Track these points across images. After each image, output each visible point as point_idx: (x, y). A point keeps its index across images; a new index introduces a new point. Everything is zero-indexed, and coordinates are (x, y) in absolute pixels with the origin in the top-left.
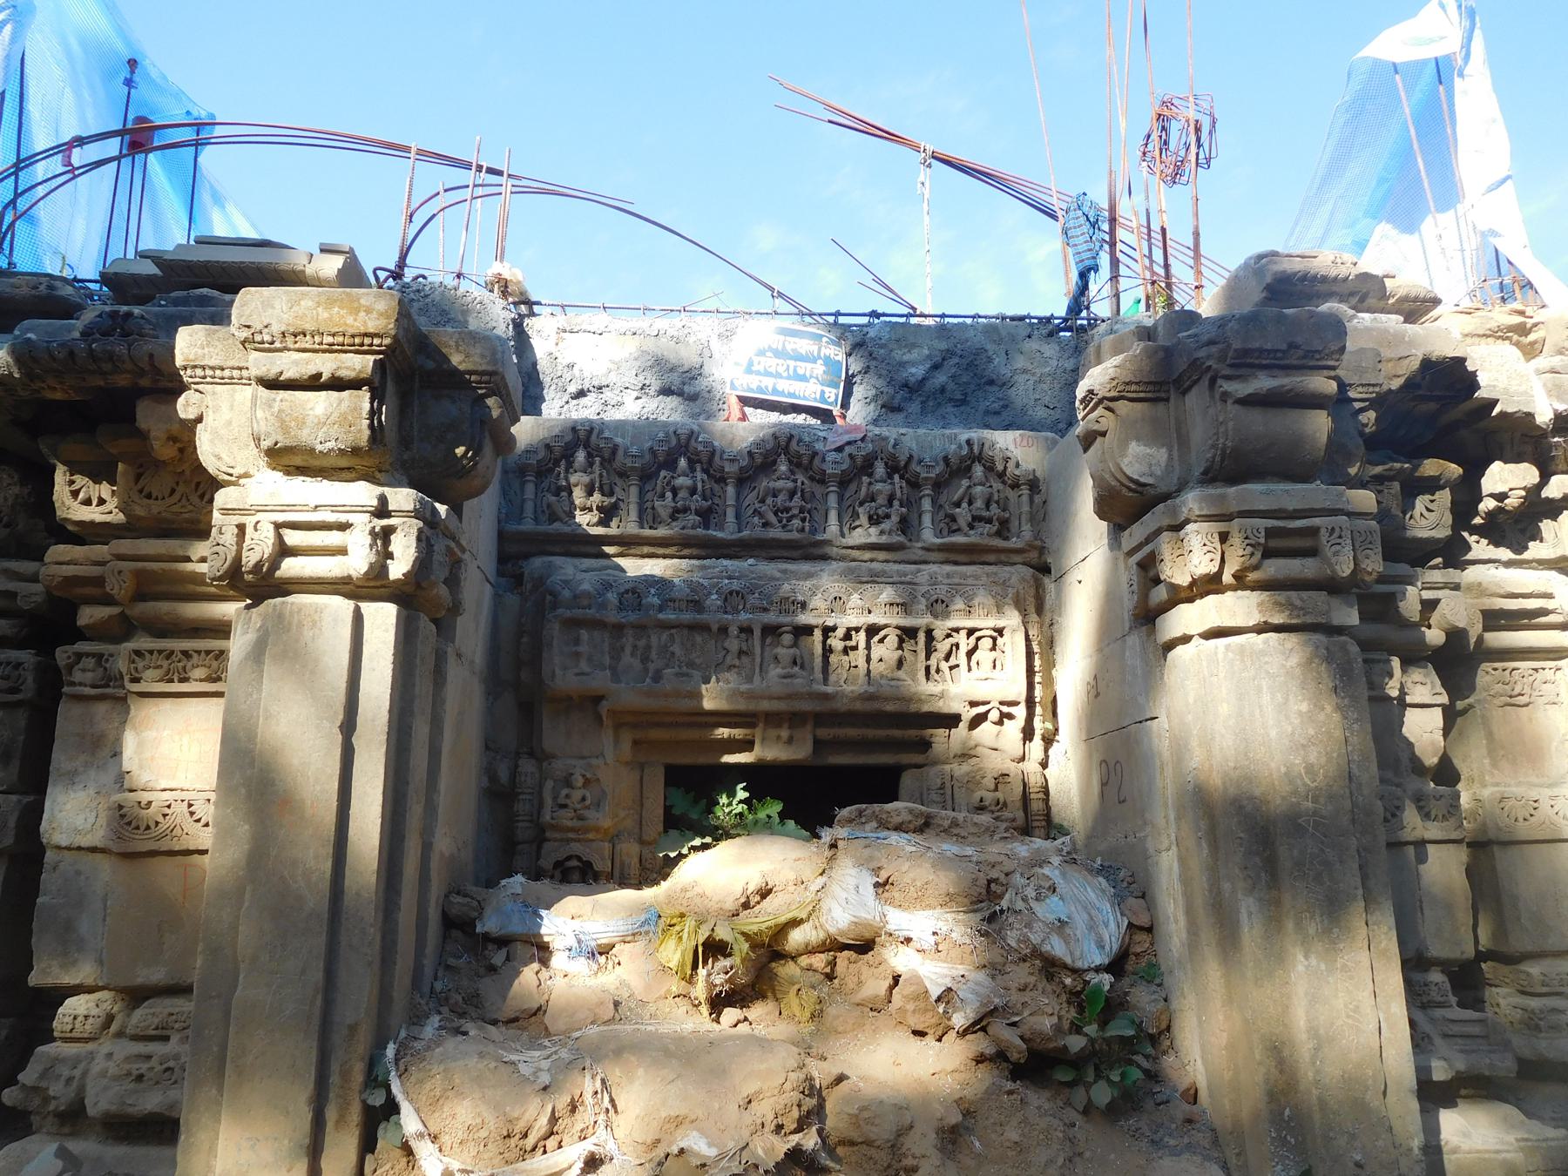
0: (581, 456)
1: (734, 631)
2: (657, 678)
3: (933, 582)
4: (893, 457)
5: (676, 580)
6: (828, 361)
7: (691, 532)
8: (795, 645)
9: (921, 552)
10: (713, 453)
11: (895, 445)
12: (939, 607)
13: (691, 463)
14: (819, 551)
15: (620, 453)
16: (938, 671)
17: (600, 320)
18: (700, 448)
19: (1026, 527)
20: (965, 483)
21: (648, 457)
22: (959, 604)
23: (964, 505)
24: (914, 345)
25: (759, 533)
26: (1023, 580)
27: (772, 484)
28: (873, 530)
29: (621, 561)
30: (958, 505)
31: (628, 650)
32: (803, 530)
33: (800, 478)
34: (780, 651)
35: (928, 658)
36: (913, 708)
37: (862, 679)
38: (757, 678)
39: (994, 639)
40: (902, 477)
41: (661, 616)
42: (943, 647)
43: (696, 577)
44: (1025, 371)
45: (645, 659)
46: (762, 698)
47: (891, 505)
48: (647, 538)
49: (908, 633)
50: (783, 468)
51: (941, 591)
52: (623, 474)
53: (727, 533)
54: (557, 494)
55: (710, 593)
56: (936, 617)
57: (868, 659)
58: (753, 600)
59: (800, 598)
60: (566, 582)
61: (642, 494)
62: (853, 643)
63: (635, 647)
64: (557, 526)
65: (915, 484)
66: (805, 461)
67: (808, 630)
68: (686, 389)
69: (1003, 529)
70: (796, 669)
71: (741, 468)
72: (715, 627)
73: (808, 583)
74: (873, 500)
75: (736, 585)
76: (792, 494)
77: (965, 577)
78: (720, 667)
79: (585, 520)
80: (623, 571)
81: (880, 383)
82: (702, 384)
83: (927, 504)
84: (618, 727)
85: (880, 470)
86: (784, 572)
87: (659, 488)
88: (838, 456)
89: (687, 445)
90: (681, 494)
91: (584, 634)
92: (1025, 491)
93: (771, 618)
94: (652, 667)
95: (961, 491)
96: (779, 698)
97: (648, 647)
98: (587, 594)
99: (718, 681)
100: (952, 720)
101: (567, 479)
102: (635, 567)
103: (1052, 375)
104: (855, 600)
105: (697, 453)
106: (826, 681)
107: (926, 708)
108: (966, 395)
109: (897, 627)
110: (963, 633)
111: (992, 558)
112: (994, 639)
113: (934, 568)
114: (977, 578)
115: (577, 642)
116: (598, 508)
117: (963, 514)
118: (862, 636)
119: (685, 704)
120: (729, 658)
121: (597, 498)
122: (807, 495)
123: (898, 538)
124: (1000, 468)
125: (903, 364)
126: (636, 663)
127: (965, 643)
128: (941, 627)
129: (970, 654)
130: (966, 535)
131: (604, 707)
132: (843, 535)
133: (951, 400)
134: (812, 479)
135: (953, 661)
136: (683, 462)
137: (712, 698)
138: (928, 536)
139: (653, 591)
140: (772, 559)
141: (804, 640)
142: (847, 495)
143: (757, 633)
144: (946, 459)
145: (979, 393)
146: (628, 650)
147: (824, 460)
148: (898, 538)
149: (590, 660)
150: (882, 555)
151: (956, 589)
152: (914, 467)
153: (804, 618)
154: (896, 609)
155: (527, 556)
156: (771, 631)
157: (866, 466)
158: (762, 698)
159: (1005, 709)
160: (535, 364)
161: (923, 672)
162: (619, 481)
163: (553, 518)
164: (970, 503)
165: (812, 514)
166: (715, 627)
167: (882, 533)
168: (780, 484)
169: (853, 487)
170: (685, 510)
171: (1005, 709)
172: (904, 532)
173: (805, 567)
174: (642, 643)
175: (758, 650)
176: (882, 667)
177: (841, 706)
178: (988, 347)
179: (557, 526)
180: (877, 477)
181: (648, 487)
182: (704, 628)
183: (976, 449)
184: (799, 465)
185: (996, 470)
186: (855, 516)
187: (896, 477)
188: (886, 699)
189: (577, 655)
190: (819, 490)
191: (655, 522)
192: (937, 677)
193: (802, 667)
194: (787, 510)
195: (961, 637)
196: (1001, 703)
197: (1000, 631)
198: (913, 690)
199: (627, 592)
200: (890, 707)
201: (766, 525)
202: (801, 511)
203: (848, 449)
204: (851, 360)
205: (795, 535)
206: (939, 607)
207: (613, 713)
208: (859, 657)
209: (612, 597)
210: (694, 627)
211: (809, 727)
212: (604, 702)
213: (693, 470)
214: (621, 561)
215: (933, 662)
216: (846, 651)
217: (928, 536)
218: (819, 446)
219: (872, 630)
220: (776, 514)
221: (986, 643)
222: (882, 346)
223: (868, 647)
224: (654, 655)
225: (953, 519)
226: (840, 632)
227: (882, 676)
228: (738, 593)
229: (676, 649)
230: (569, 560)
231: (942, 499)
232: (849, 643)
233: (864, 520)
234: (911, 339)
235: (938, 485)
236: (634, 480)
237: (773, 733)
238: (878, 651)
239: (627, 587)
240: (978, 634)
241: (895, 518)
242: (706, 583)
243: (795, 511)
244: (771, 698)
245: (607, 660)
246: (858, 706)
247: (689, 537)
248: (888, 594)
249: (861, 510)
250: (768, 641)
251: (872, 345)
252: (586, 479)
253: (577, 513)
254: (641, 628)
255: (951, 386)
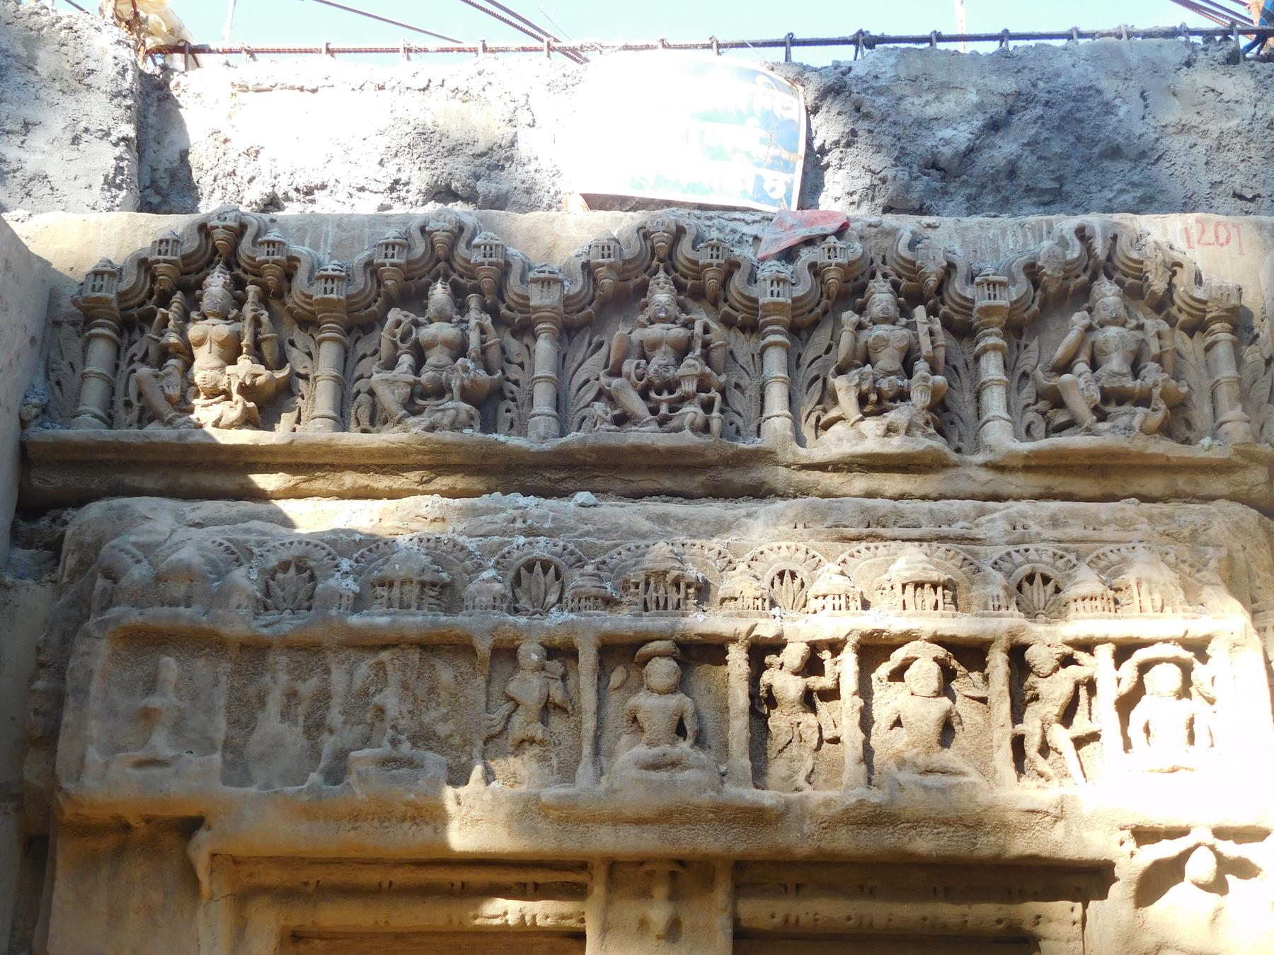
0: (216, 284)
1: (531, 653)
2: (337, 772)
3: (1019, 536)
4: (912, 269)
5: (402, 540)
6: (768, 119)
7: (448, 436)
8: (681, 686)
9: (984, 475)
10: (506, 268)
11: (912, 245)
12: (1036, 588)
13: (459, 294)
14: (740, 478)
15: (302, 274)
16: (1045, 749)
17: (314, 69)
18: (477, 257)
19: (1233, 414)
20: (1079, 319)
21: (361, 280)
22: (1087, 582)
23: (1081, 367)
24: (946, 87)
25: (595, 431)
26: (1238, 528)
27: (638, 335)
28: (872, 426)
29: (289, 507)
30: (1065, 367)
31: (275, 703)
32: (706, 428)
33: (701, 318)
34: (645, 702)
35: (1017, 715)
36: (986, 846)
37: (852, 769)
38: (585, 770)
39: (1186, 669)
40: (932, 312)
41: (355, 620)
42: (1055, 689)
43: (453, 530)
44: (1184, 129)
45: (316, 727)
46: (596, 819)
47: (909, 373)
48: (350, 452)
49: (965, 654)
50: (661, 296)
51: (1041, 557)
52: (308, 323)
53: (536, 435)
54: (160, 364)
55: (480, 568)
56: (1031, 614)
57: (866, 722)
58: (578, 580)
59: (693, 573)
60: (148, 549)
61: (347, 361)
62: (825, 682)
63: (292, 695)
64: (155, 431)
65: (962, 329)
66: (711, 280)
67: (710, 650)
68: (482, 186)
69: (1177, 421)
70: (684, 746)
71: (567, 300)
72: (484, 646)
73: (717, 543)
74: (867, 360)
75: (542, 547)
76: (682, 351)
77: (1097, 524)
78: (494, 742)
79: (217, 421)
80: (287, 523)
81: (880, 162)
82: (514, 177)
83: (992, 368)
84: (244, 897)
85: (881, 296)
86: (663, 519)
87: (385, 350)
88: (786, 271)
89: (449, 260)
90: (434, 357)
91: (170, 666)
92: (1222, 334)
93: (623, 621)
94: (329, 744)
95: (1073, 336)
96: (639, 821)
97: (323, 698)
98: (186, 572)
99: (489, 776)
100: (1090, 879)
101: (182, 333)
102: (315, 515)
103: (1246, 134)
104: (828, 579)
105: (470, 272)
106: (759, 775)
107: (1020, 846)
108: (1060, 179)
109: (938, 640)
110: (1105, 653)
111: (1155, 484)
112: (1186, 669)
113: (1015, 507)
114: (1125, 524)
115: (152, 685)
116: (243, 389)
117: (1080, 388)
118: (849, 658)
119: (405, 839)
120: (518, 720)
121: (244, 367)
122: (717, 355)
123: (924, 443)
124: (1158, 285)
125: (924, 124)
126: (294, 736)
127: (1112, 680)
128: (1044, 642)
129: (1126, 705)
130: (1089, 431)
131: (202, 848)
132: (800, 441)
133: (1029, 190)
134: (728, 322)
135: (1081, 725)
136: (439, 293)
137: (475, 818)
138: (1000, 435)
139: (345, 564)
140: (637, 496)
141: (704, 674)
142: (809, 355)
143: (588, 657)
144: (1032, 270)
145: (1091, 176)
146: (275, 703)
147: (752, 279)
148: (924, 443)
149: (178, 728)
150: (894, 483)
151: (1074, 552)
152: (958, 286)
153: (701, 622)
154: (929, 596)
155: (81, 501)
156: (621, 653)
157: (851, 290)
158: (596, 819)
159: (1230, 849)
160: (184, 154)
161: (1006, 752)
162: (299, 336)
163: (147, 415)
164: (1094, 365)
165: (724, 394)
166: (484, 646)
167: (890, 430)
168: (657, 331)
169: (821, 338)
170: (440, 391)
171: (1230, 849)
172: (940, 431)
173: (713, 509)
174: (308, 687)
175: (588, 699)
176: (901, 739)
177: (799, 840)
178: (1104, 84)
179: (155, 431)
180: (875, 310)
181: (362, 348)
182: (460, 648)
183: (1100, 247)
184: (698, 294)
185: (1149, 293)
186: (828, 397)
187: (920, 312)
188: (916, 823)
189: (148, 716)
190: (744, 346)
191: (377, 418)
192: (1042, 764)
193: (700, 741)
194: (671, 386)
195: (1100, 664)
196: (1220, 833)
197: (1199, 648)
198: (983, 798)
199: (285, 566)
200: (924, 844)
201: (622, 420)
202: (703, 386)
203: (807, 255)
204: (816, 121)
205: (687, 439)
206: (1038, 593)
207: (226, 862)
208: (841, 717)
209: (244, 579)
210: (431, 646)
211: (721, 896)
212: (202, 835)
213: (462, 308)
214: (289, 507)
215: (1031, 727)
216: (808, 700)
217: (1000, 435)
218: (745, 253)
219: (873, 650)
220: (644, 395)
221: (1164, 679)
222: (880, 92)
223: (865, 690)
224: (335, 716)
225: (1056, 400)
226: (794, 654)
227: (902, 763)
228: (546, 566)
229: (391, 700)
230: (168, 503)
231: (1028, 360)
232: (816, 682)
233: (847, 403)
234: (940, 76)
235: (1018, 329)
236: (330, 330)
237: (629, 910)
238: (889, 700)
239: (286, 555)
240: (1140, 655)
241: (920, 398)
242: (471, 544)
243: (689, 387)
244: (617, 820)
245: (220, 727)
246: (844, 841)
247: (445, 449)
248: (909, 561)
249: (840, 383)
250: (616, 677)
251: (862, 92)
252: (221, 329)
253: (198, 402)
254: (308, 651)
255: (1028, 162)
